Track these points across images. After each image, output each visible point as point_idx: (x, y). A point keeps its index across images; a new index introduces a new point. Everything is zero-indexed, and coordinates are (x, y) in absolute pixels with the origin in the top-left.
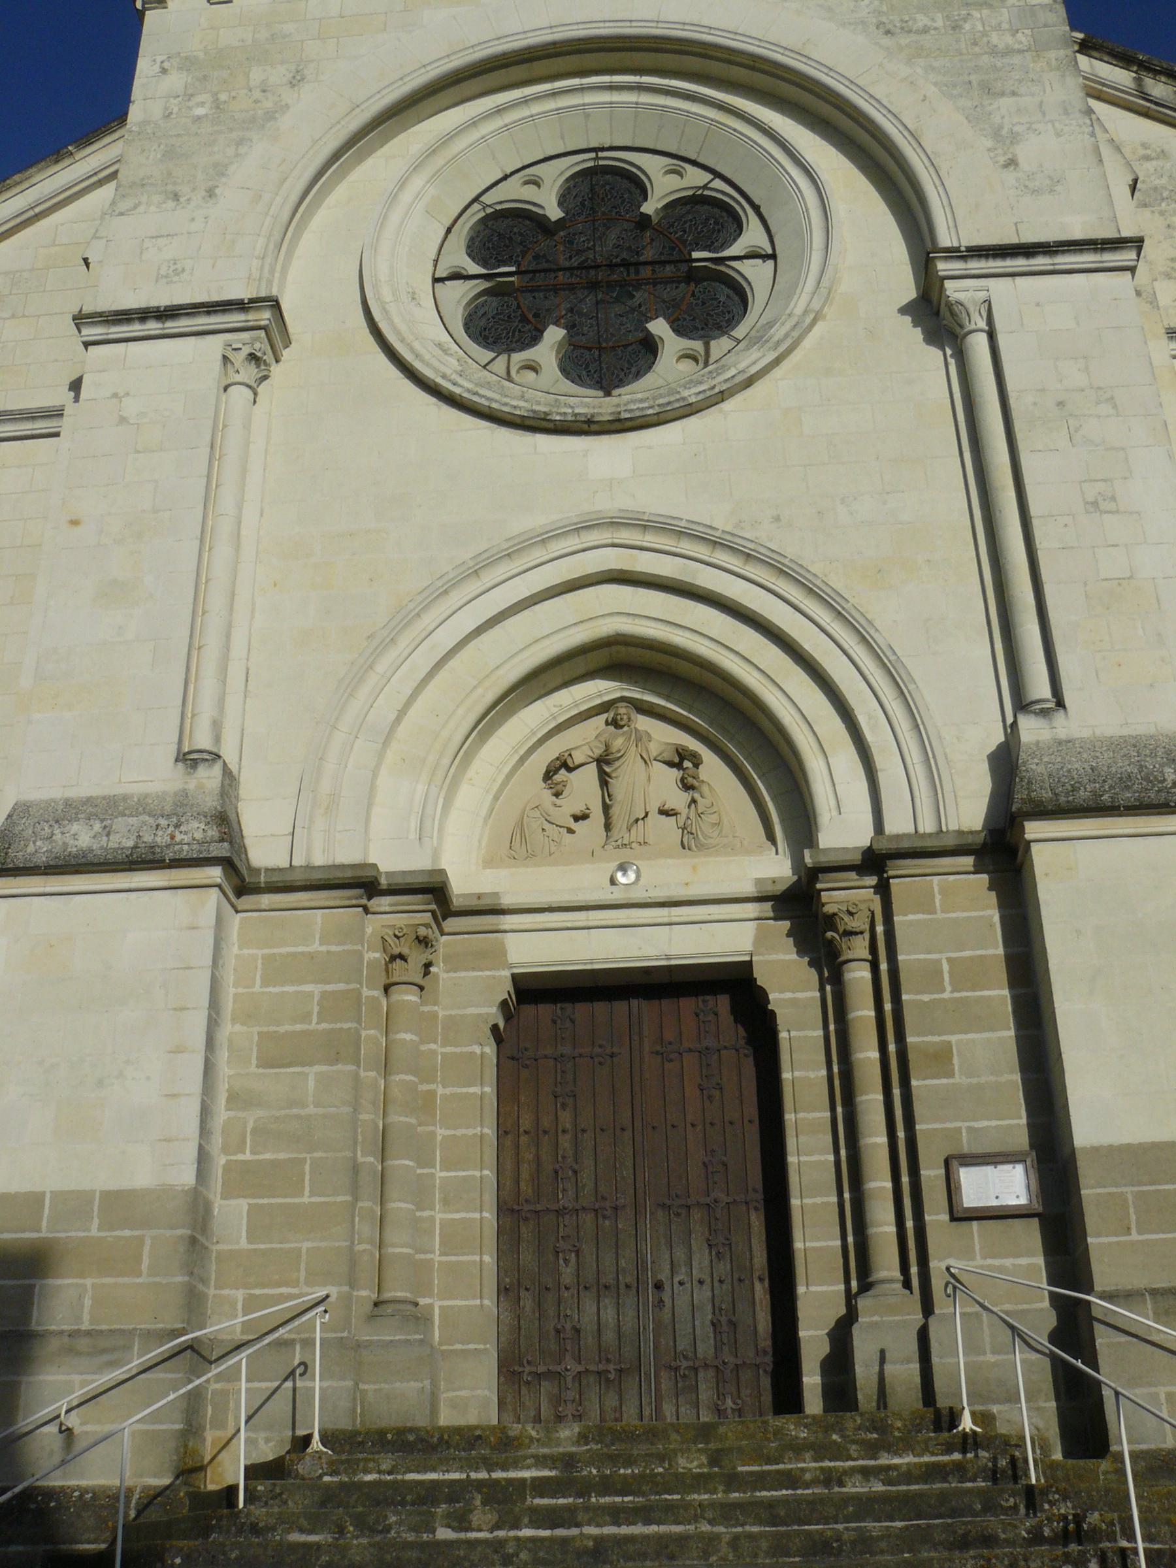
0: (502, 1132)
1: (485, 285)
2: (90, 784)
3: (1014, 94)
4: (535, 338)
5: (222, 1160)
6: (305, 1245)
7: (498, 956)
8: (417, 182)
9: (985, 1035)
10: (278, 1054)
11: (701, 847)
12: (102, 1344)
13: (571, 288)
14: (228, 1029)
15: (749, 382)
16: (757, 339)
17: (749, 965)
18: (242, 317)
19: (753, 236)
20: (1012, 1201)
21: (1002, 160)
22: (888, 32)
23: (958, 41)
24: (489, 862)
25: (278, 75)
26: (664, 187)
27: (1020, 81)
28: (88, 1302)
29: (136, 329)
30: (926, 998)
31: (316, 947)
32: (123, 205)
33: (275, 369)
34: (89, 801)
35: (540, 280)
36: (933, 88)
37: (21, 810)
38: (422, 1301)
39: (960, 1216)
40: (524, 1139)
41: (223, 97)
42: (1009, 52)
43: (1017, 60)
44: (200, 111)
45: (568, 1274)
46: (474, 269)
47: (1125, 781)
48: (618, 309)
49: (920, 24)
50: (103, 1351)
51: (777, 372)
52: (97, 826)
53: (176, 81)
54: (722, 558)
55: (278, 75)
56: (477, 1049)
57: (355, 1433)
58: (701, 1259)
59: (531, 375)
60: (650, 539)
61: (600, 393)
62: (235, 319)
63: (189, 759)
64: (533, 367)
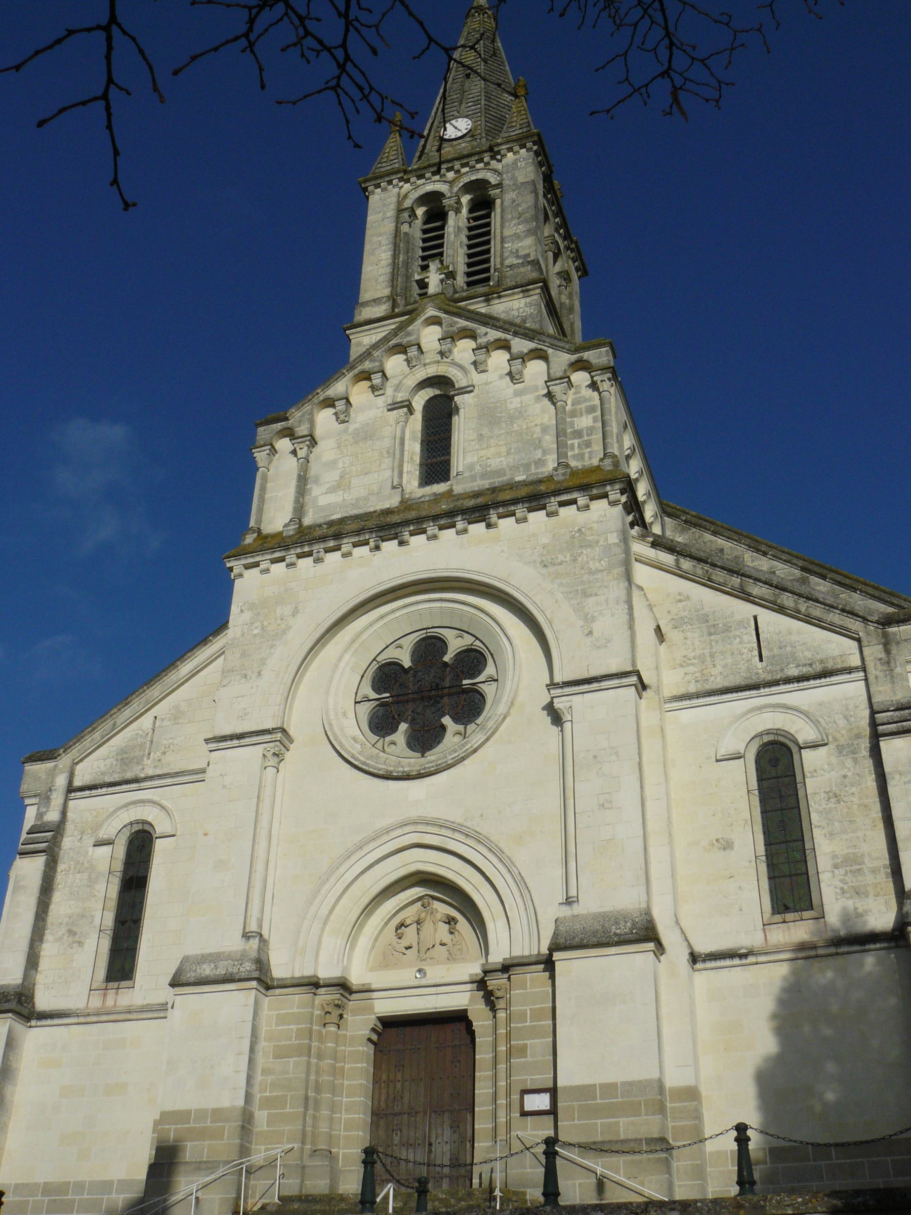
0: (376, 1080)
1: (378, 703)
2: (210, 948)
3: (596, 595)
4: (394, 730)
5: (259, 1096)
6: (287, 1128)
7: (370, 1009)
8: (347, 657)
9: (542, 1040)
10: (280, 1054)
11: (454, 960)
12: (202, 1166)
13: (414, 700)
14: (262, 1044)
15: (475, 751)
16: (482, 727)
17: (466, 1010)
18: (270, 736)
19: (490, 670)
20: (545, 1108)
21: (586, 632)
22: (545, 566)
23: (575, 567)
24: (372, 970)
25: (287, 610)
26: (455, 644)
27: (599, 587)
28: (206, 1150)
29: (229, 744)
30: (520, 1025)
31: (295, 1010)
32: (225, 682)
33: (288, 755)
34: (210, 955)
35: (401, 698)
36: (561, 595)
37: (185, 959)
38: (333, 1150)
39: (524, 1114)
40: (383, 1085)
41: (265, 623)
42: (598, 571)
43: (599, 576)
44: (256, 632)
45: (396, 1139)
46: (373, 695)
47: (595, 933)
48: (433, 710)
49: (559, 560)
50: (210, 1168)
51: (488, 744)
52: (213, 966)
53: (247, 616)
54: (457, 836)
55: (287, 610)
56: (361, 1048)
57: (292, 1196)
58: (448, 1133)
59: (393, 746)
60: (429, 829)
61: (419, 755)
62: (267, 737)
63: (246, 936)
64: (394, 743)
